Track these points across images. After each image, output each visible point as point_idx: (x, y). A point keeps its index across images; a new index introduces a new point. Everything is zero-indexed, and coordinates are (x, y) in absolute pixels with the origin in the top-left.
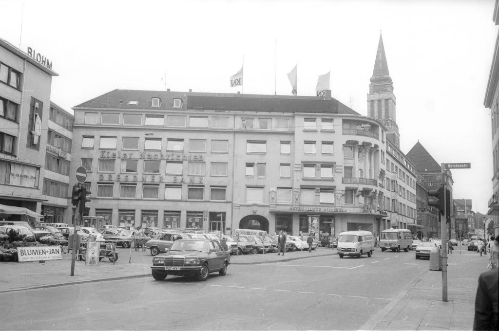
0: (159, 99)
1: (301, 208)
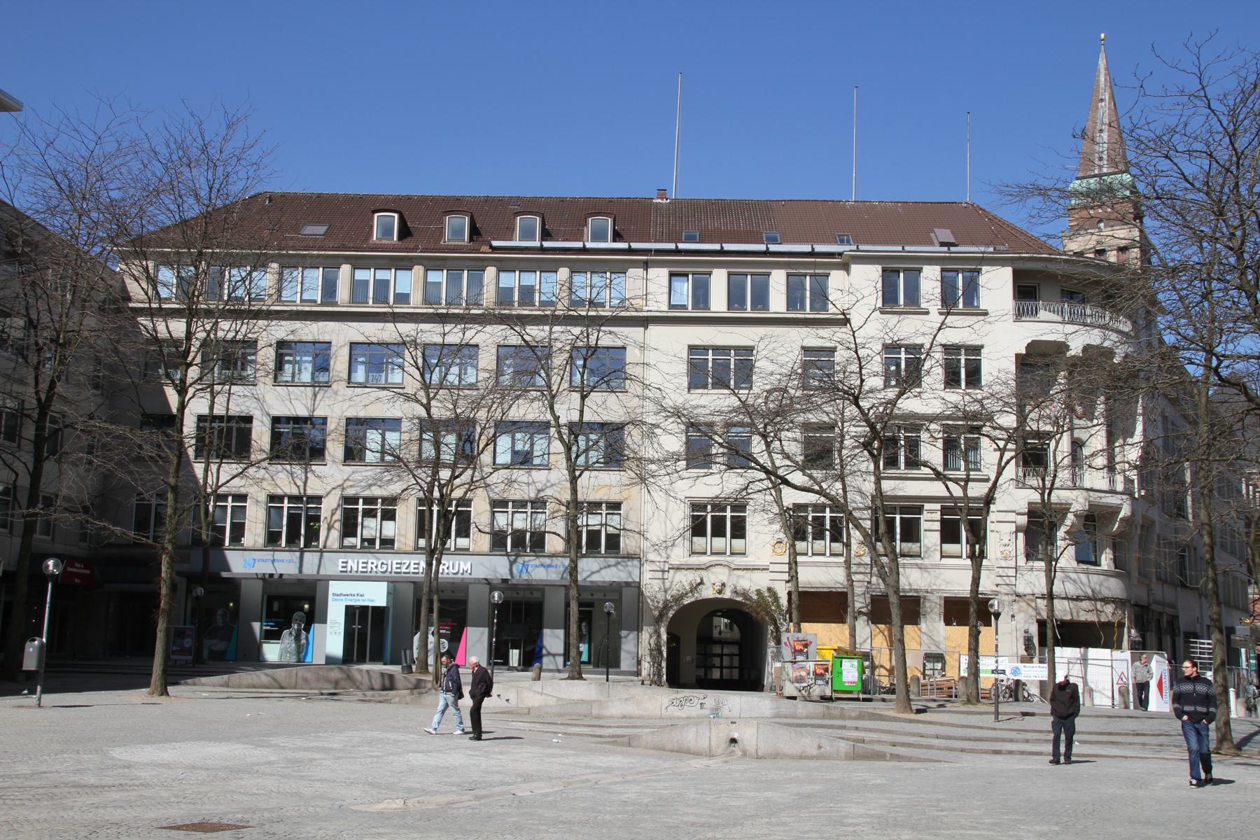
0: (396, 216)
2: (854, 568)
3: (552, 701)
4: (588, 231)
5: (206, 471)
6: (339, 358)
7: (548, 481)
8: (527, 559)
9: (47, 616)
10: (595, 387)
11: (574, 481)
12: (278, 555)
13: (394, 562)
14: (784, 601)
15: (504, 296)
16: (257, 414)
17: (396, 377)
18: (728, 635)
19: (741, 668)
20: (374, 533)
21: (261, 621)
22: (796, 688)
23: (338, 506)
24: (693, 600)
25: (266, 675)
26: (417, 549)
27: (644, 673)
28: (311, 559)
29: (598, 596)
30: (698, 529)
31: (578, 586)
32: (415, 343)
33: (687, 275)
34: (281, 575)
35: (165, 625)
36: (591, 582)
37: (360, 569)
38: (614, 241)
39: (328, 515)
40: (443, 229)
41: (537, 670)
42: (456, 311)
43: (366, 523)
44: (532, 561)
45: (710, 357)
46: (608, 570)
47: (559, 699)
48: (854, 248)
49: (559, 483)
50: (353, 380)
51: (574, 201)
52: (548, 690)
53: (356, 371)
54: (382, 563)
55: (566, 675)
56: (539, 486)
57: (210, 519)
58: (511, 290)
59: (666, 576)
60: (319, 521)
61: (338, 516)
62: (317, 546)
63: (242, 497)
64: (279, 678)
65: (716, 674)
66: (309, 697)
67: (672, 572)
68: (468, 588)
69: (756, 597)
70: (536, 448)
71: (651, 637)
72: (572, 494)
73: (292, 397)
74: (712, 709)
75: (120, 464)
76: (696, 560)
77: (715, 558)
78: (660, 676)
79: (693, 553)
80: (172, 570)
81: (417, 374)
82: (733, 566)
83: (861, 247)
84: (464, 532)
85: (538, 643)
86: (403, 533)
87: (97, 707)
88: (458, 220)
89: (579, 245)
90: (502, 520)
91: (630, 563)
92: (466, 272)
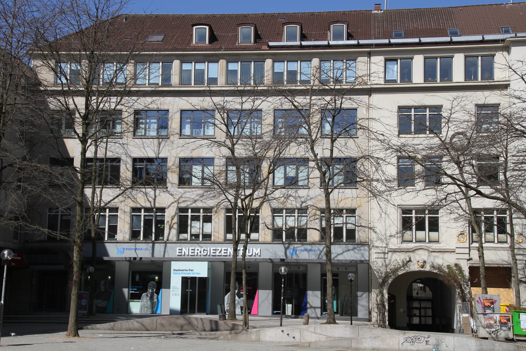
0: (207, 27)
2: (516, 251)
3: (323, 338)
4: (330, 34)
5: (94, 193)
6: (174, 120)
7: (308, 196)
8: (296, 246)
9: (4, 286)
10: (340, 135)
11: (327, 195)
12: (139, 246)
13: (212, 249)
14: (467, 273)
15: (277, 77)
16: (123, 157)
17: (210, 131)
18: (422, 295)
19: (433, 317)
20: (198, 231)
21: (128, 288)
22: (487, 331)
23: (176, 214)
24: (404, 272)
25: (138, 322)
26: (226, 240)
27: (374, 319)
28: (159, 247)
29: (342, 269)
30: (406, 224)
31: (331, 263)
32: (223, 108)
33: (396, 60)
34: (141, 258)
35: (76, 291)
36: (338, 260)
37: (190, 254)
38: (348, 39)
39: (170, 220)
40: (237, 35)
41: (307, 318)
42: (249, 88)
43: (193, 225)
44: (299, 247)
45: (413, 113)
46: (348, 252)
47: (328, 337)
48: (514, 35)
49: (315, 197)
50: (183, 133)
51: (320, 14)
52: (319, 331)
53: (185, 128)
54: (204, 250)
55: (325, 321)
56: (303, 200)
57: (96, 223)
58: (282, 73)
59: (386, 256)
60: (164, 224)
61: (176, 220)
62: (163, 240)
63: (116, 209)
64: (145, 324)
65: (416, 320)
66: (166, 336)
67: (390, 254)
68: (258, 265)
69: (447, 270)
70: (300, 175)
71: (377, 296)
72: (326, 204)
73: (145, 145)
74: (434, 345)
75: (45, 189)
76: (405, 246)
77: (418, 244)
78: (384, 322)
79: (404, 241)
80: (80, 255)
81: (224, 128)
82: (430, 250)
83: (518, 35)
84: (255, 229)
85: (304, 300)
86: (217, 230)
87: (36, 345)
88: (247, 29)
89: (325, 43)
90: (279, 222)
91: (362, 248)
92: (253, 63)
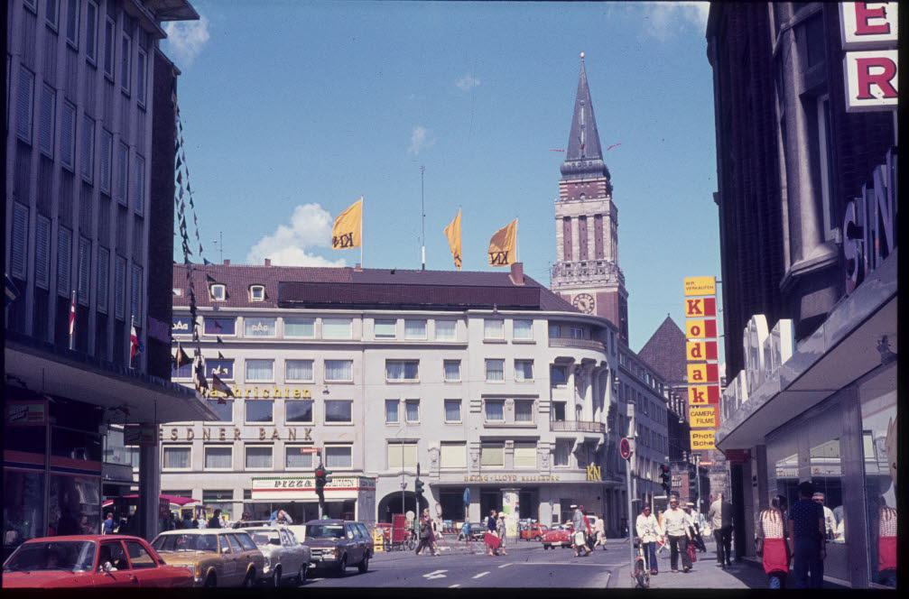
0: (223, 287)
1: (483, 475)
